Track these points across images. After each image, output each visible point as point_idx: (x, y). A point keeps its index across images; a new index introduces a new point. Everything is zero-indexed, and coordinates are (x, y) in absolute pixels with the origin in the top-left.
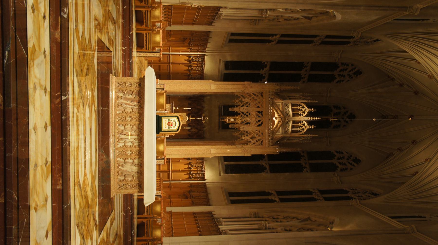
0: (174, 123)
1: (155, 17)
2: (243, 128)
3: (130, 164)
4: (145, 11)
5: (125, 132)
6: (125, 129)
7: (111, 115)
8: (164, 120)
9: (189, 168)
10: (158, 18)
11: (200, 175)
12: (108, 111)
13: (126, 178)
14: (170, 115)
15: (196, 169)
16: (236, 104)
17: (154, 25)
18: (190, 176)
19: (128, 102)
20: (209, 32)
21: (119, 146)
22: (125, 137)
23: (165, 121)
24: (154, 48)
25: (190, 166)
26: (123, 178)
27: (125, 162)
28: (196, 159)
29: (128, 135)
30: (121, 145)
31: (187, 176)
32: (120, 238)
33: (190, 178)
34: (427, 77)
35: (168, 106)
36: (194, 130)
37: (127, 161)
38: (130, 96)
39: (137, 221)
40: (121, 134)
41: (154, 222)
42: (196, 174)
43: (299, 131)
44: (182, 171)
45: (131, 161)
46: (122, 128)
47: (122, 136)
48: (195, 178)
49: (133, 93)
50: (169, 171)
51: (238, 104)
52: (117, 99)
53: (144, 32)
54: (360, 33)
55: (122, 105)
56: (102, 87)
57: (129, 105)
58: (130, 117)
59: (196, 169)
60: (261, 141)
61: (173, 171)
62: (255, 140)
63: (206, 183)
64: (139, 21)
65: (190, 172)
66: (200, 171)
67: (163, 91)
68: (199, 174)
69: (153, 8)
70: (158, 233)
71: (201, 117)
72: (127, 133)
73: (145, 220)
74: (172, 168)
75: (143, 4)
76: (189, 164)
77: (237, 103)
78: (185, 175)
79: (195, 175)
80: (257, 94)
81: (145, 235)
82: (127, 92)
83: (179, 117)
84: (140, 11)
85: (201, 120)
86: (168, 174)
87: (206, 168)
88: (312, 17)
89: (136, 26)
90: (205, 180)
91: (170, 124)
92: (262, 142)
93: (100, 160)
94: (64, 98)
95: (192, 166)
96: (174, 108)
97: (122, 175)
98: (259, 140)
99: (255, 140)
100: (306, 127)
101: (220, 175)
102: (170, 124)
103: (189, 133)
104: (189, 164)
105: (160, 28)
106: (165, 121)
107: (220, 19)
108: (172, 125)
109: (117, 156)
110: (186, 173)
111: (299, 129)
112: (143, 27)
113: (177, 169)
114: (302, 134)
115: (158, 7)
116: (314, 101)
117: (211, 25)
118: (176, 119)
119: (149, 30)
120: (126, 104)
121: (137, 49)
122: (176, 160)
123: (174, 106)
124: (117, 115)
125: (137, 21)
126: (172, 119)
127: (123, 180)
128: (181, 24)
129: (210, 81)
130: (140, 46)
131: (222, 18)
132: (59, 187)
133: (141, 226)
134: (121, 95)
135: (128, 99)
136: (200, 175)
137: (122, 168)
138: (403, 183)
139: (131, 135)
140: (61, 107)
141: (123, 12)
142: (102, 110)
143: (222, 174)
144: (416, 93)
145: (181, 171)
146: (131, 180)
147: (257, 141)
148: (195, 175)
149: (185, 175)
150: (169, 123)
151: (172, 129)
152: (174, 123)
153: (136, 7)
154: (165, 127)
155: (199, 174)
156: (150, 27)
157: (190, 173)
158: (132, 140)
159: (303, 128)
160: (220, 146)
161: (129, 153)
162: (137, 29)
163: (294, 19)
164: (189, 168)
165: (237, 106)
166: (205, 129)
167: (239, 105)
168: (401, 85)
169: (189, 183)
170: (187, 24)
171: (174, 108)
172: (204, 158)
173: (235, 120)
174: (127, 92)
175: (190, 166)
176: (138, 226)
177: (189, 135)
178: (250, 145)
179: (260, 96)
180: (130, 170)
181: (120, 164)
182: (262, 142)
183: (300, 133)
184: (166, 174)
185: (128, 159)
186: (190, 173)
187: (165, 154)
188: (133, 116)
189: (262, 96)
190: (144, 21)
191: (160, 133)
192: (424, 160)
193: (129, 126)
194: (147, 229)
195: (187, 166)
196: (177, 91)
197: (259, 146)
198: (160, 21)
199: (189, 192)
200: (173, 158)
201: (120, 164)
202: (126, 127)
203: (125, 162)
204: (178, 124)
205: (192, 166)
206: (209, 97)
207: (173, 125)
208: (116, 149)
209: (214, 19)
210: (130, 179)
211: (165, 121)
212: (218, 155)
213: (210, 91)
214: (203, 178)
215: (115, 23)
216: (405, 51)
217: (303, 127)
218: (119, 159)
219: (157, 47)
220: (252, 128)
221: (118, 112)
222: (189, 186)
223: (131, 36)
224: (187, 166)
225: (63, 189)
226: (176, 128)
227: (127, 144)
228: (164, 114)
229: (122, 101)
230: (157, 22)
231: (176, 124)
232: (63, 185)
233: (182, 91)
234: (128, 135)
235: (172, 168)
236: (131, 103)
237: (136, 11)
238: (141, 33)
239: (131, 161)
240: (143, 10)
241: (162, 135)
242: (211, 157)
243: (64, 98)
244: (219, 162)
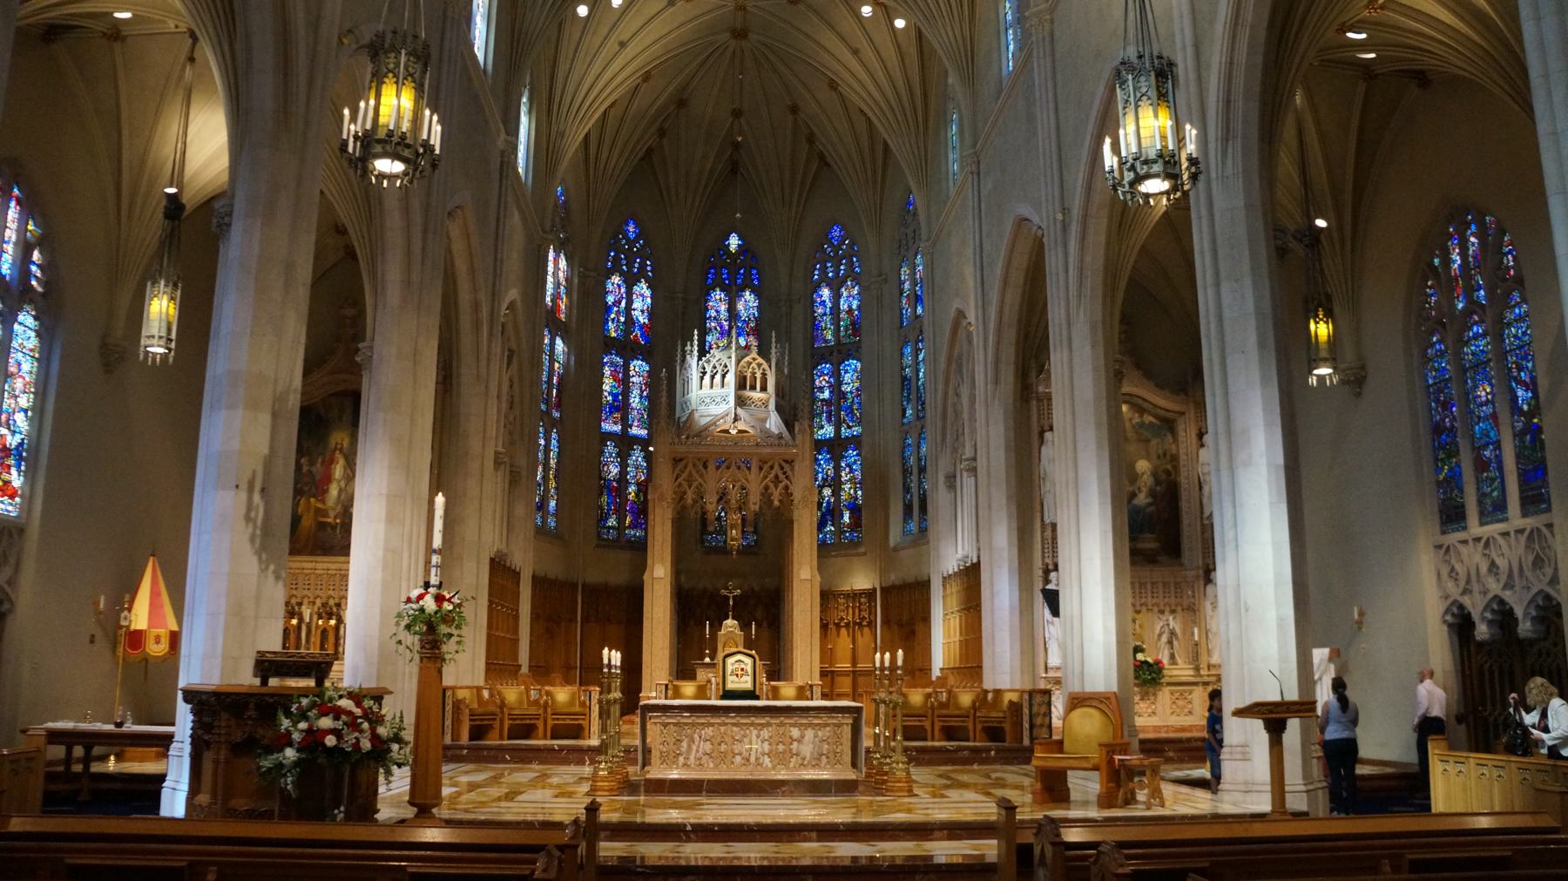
0: (736, 666)
1: (571, 703)
2: (755, 502)
3: (801, 746)
4: (510, 719)
5: (745, 754)
6: (740, 754)
7: (716, 777)
8: (730, 686)
9: (847, 625)
10: (521, 693)
11: (863, 600)
12: (709, 781)
13: (825, 752)
14: (721, 673)
15: (850, 610)
16: (700, 513)
17: (536, 702)
18: (865, 623)
19: (694, 748)
20: (533, 577)
21: (770, 765)
22: (753, 753)
23: (732, 682)
24: (583, 704)
25: (842, 624)
26: (824, 757)
27: (797, 755)
28: (822, 611)
29: (751, 749)
30: (767, 760)
31: (866, 630)
32: (953, 771)
33: (872, 624)
34: (645, 84)
35: (702, 675)
36: (759, 614)
37: (794, 752)
38: (685, 744)
39: (939, 741)
40: (748, 760)
41: (942, 705)
42: (860, 611)
43: (764, 375)
44: (854, 642)
45: (795, 744)
46: (738, 759)
47: (753, 759)
48: (870, 614)
49: (678, 740)
50: (854, 672)
51: (699, 510)
52: (689, 766)
53: (550, 723)
54: (545, 236)
55: (700, 759)
56: (669, 792)
57: (699, 746)
58: (720, 745)
59: (850, 610)
60: (783, 464)
61: (854, 662)
62: (782, 477)
63: (882, 589)
64: (527, 731)
65: (855, 623)
66: (854, 602)
67: (670, 686)
68: (860, 604)
69: (503, 705)
70: (966, 699)
71: (727, 598)
72: (747, 751)
73: (937, 726)
74: (845, 665)
75: (497, 724)
76: (838, 626)
77: (696, 513)
78: (862, 635)
79: (863, 613)
80: (677, 472)
81: (1003, 725)
82: (678, 749)
83: (726, 652)
84: (509, 729)
85: (734, 597)
86: (861, 675)
87: (847, 588)
88: (509, 350)
89: (538, 739)
90: (875, 589)
91: (740, 673)
92: (786, 461)
93: (791, 794)
94: (689, 828)
95: (842, 619)
96: (707, 660)
97: (819, 759)
98: (782, 468)
99: (782, 477)
100: (754, 359)
101: (865, 554)
102: (740, 673)
103: (765, 624)
104: (838, 626)
105: (540, 690)
106: (733, 684)
107: (506, 555)
108: (742, 670)
109: (788, 768)
110: (858, 634)
111: (758, 375)
112: (540, 724)
113: (849, 654)
114: (770, 367)
115: (499, 693)
116: (696, 337)
117: (519, 573)
118: (730, 661)
119: (545, 712)
120: (697, 751)
121: (584, 739)
122: (827, 655)
123: (703, 659)
124: (716, 766)
125: (526, 737)
126: (729, 668)
127: (828, 757)
128: (515, 642)
129: (645, 577)
130: (577, 732)
131: (505, 551)
132: (814, 835)
133: (950, 733)
134: (681, 759)
135: (689, 748)
136: (863, 600)
137: (808, 758)
138: (886, 144)
139: (751, 743)
140: (702, 831)
141: (516, 762)
142: (707, 792)
143: (862, 550)
144: (682, 103)
145: (854, 643)
146: (828, 744)
147: (784, 473)
148: (863, 613)
149: (862, 635)
150: (737, 675)
151: (749, 668)
152: (736, 666)
153: (501, 738)
154: (746, 683)
155: (860, 604)
156: (541, 712)
157: (860, 624)
158: (760, 743)
159: (756, 367)
160: (795, 557)
161: (781, 747)
162: (545, 738)
163: (511, 387)
164: (847, 625)
165: (704, 513)
166: (756, 588)
167: (702, 508)
168: (662, 133)
169: (882, 627)
170: (516, 630)
171: (707, 660)
172: (821, 592)
173: (732, 527)
174: (678, 749)
175: (842, 624)
176: (950, 739)
177: (770, 626)
178: (792, 489)
179: (681, 465)
180: (811, 746)
181: (800, 761)
182: (786, 461)
183: (768, 372)
184: (861, 680)
185: (791, 750)
186: (860, 624)
187: (801, 684)
188: (719, 740)
189: (681, 460)
190: (528, 722)
191: (757, 693)
192: (833, 93)
193: (735, 747)
194: (993, 722)
195: (843, 631)
196: (667, 653)
197: (796, 467)
198: (527, 690)
199: (901, 625)
200: (821, 663)
201: (800, 761)
202: (736, 751)
203: (797, 755)
204: (739, 657)
205: (842, 619)
206: (683, 578)
207: (743, 666)
208: (774, 768)
209: (509, 568)
210: (826, 746)
211: (732, 682)
212: (815, 562)
213: (669, 578)
214: (870, 594)
215: (545, 775)
216: (587, 136)
217: (754, 365)
218: (792, 765)
219: (580, 697)
220: (755, 483)
221: (711, 765)
222: (889, 628)
223: (562, 748)
224: (843, 631)
225: (818, 831)
226: (748, 661)
227: (767, 751)
228: (718, 684)
229: (692, 757)
230: (528, 696)
231: (740, 661)
232: (812, 831)
233: (668, 642)
234: (751, 749)
235: (845, 665)
236: (697, 743)
237: (509, 738)
238: (552, 729)
239: (795, 744)
240: (507, 723)
241: (761, 689)
242: (818, 578)
243: (689, 828)
244: (835, 556)
